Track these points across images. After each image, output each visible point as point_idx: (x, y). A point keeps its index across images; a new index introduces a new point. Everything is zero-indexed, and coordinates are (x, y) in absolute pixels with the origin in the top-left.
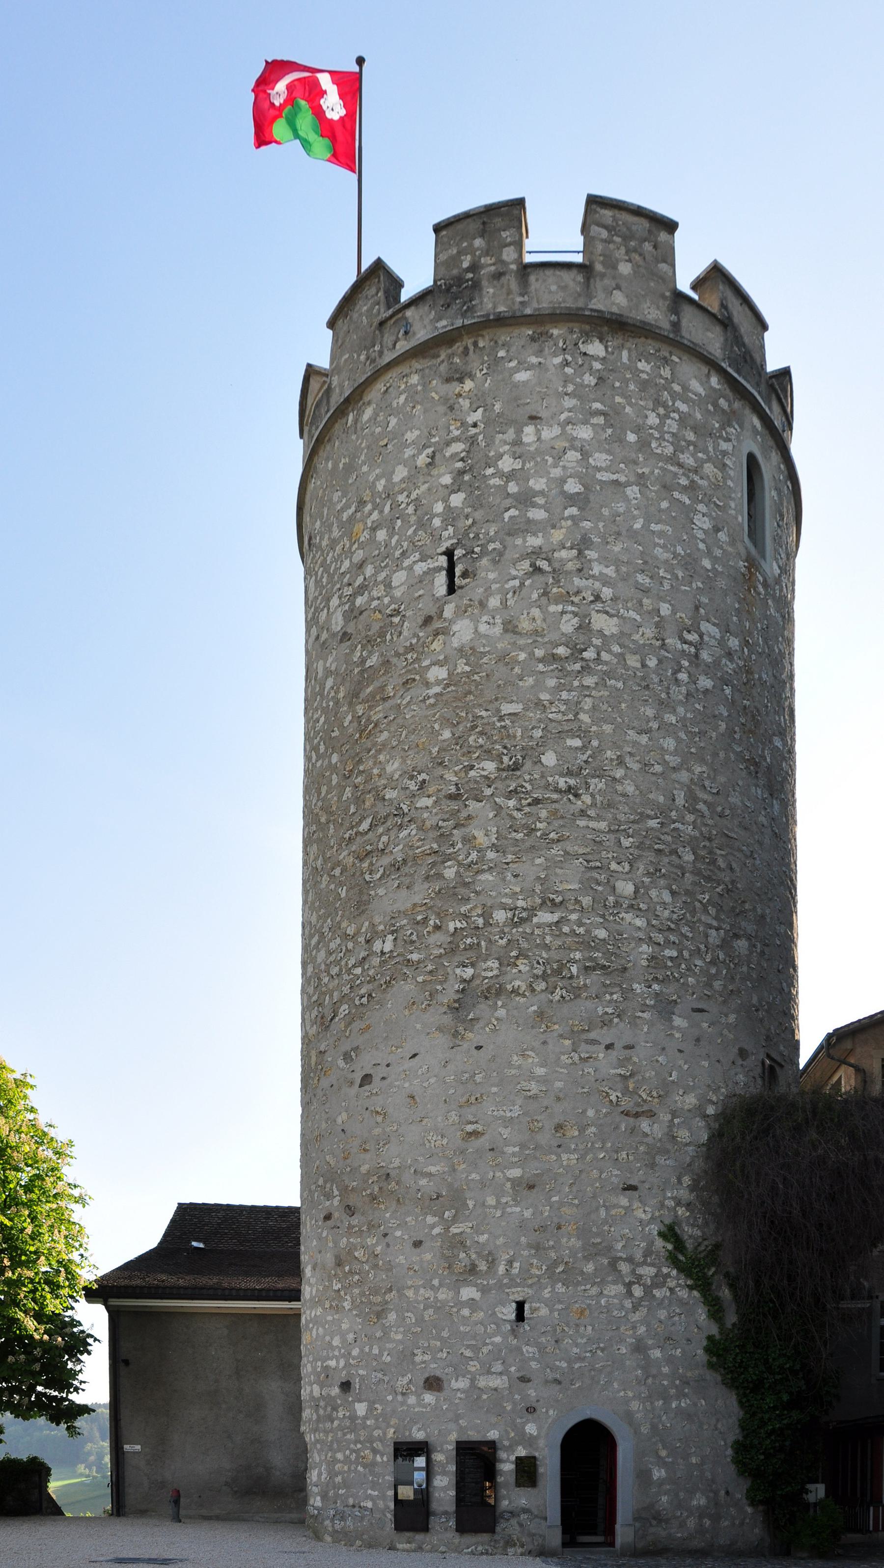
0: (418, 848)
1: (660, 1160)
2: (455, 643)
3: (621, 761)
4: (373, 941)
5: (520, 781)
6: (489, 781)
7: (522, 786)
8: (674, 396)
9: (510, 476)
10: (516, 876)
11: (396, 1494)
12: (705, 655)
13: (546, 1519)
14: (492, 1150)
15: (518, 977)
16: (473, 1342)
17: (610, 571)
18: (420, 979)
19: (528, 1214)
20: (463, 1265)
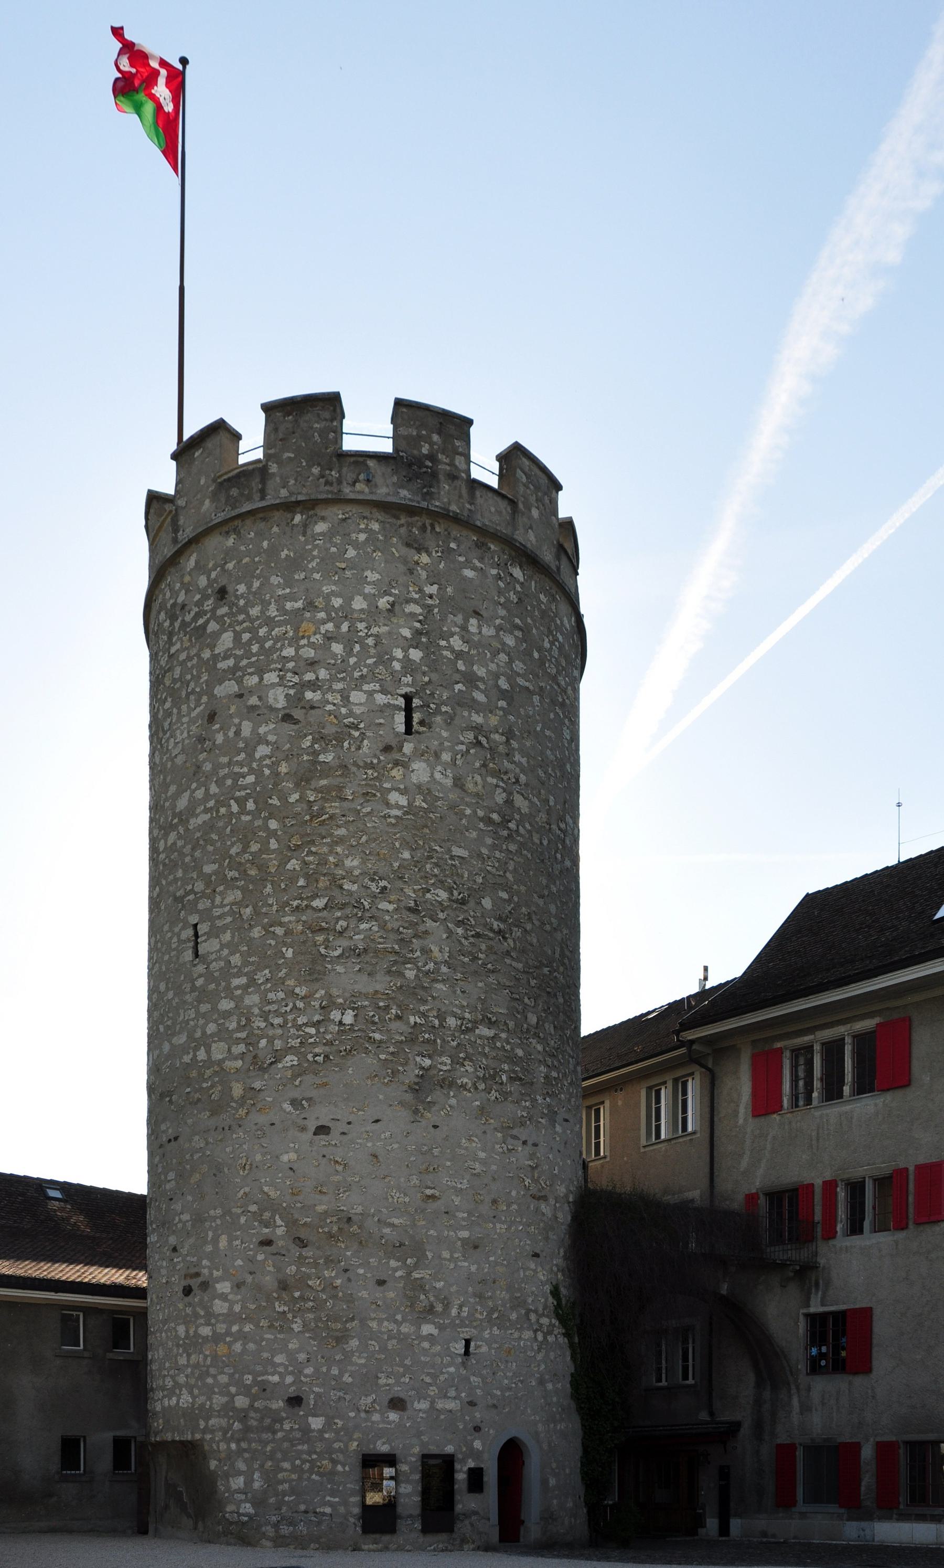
0: (380, 943)
1: (551, 1235)
2: (414, 779)
4: (329, 1009)
5: (467, 914)
7: (468, 920)
9: (459, 655)
10: (463, 992)
13: (489, 1519)
14: (447, 1213)
15: (466, 1074)
16: (432, 1371)
17: (524, 760)
18: (383, 1057)
19: (473, 1268)
20: (421, 1304)
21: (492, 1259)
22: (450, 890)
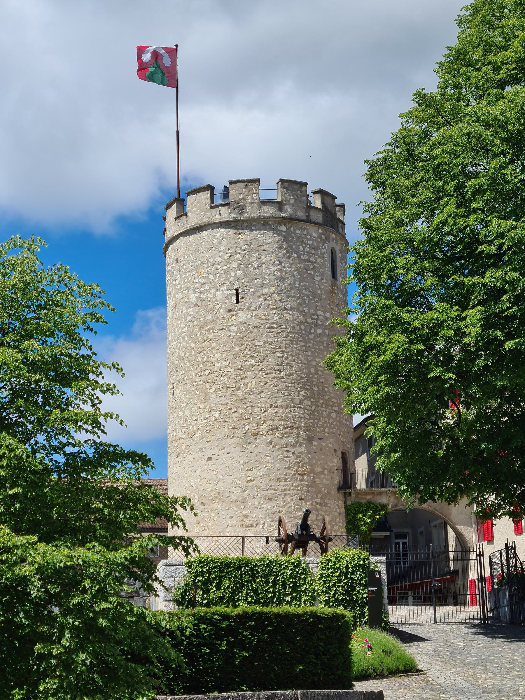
6: (252, 366)
8: (308, 239)
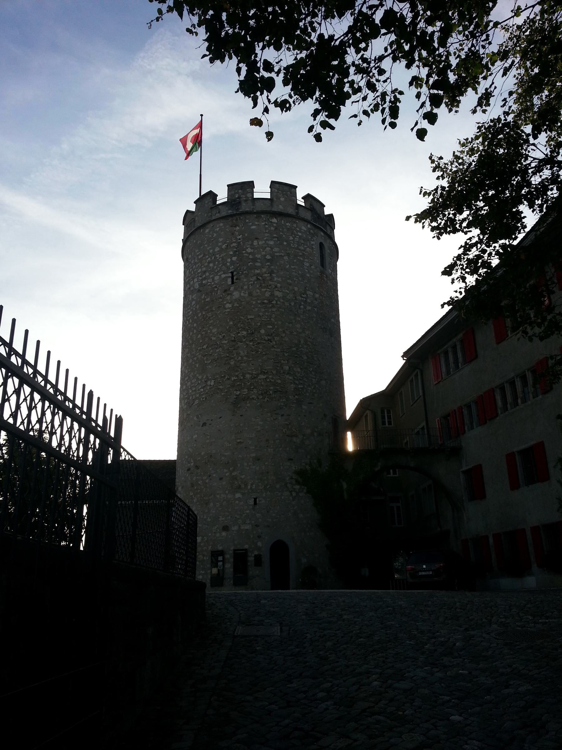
2: (234, 297)
3: (284, 332)
9: (249, 254)
11: (211, 572)
12: (308, 301)
18: (223, 394)
19: (258, 468)
21: (266, 463)
22: (247, 331)
